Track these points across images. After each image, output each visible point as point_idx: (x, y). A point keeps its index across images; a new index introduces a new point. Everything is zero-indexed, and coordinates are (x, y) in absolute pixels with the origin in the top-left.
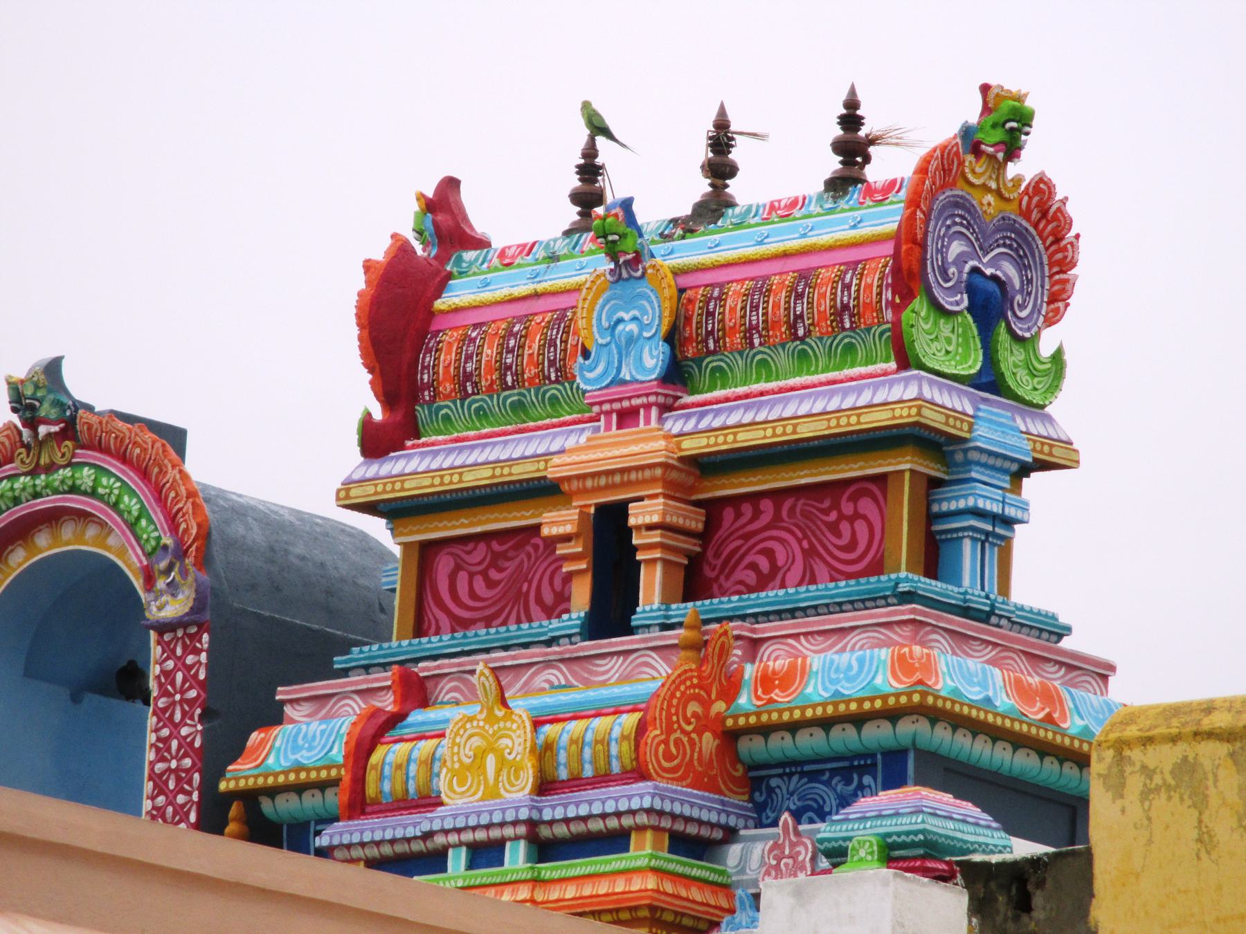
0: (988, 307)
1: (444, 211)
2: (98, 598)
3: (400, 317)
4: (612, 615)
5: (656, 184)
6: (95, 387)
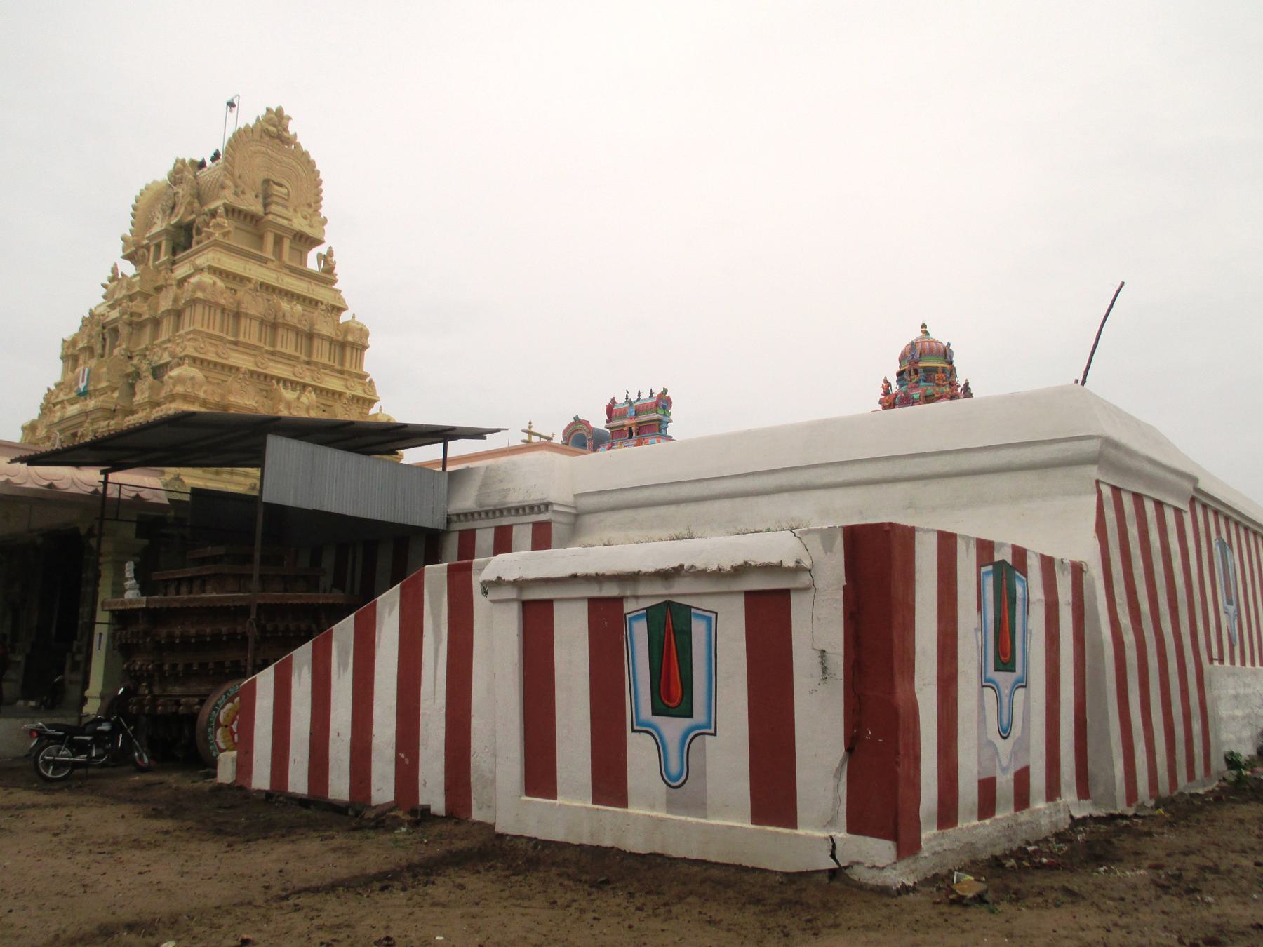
0: (664, 408)
1: (613, 400)
2: (582, 436)
3: (610, 410)
4: (631, 437)
5: (633, 397)
6: (581, 418)
